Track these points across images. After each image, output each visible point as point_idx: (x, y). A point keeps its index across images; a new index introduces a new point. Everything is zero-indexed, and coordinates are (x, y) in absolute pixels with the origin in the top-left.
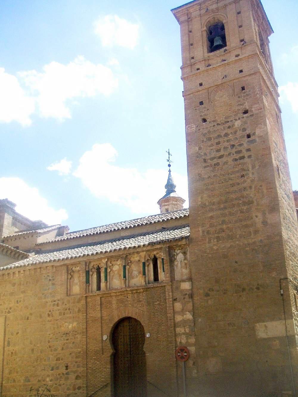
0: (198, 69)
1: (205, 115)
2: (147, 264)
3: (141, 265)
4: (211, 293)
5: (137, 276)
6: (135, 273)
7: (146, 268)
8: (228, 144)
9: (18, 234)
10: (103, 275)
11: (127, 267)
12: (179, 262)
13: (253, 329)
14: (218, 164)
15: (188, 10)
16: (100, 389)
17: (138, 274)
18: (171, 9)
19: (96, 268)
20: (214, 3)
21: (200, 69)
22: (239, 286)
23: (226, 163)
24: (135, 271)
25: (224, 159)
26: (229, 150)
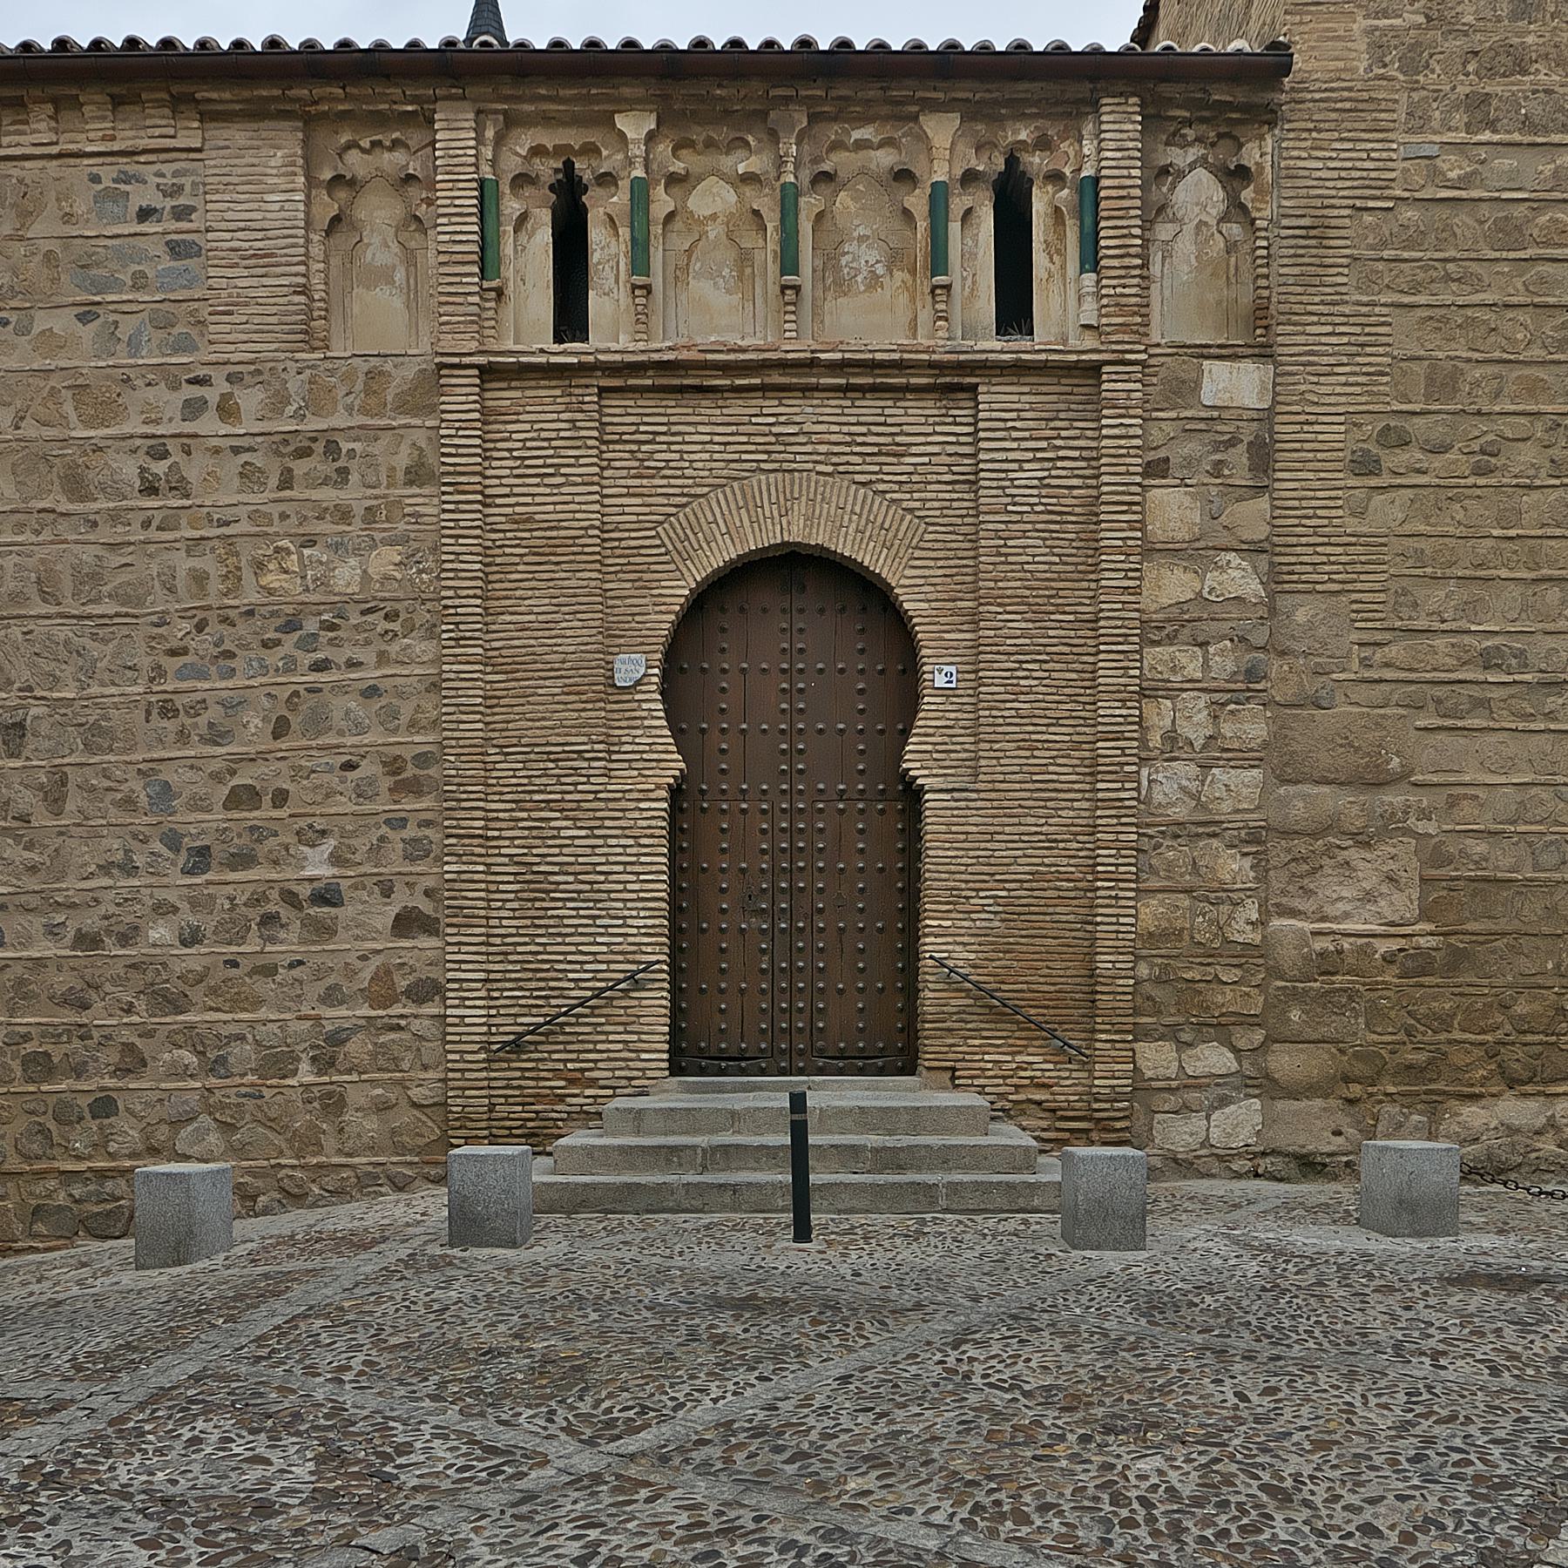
3: (917, 202)
4: (1395, 459)
5: (874, 281)
6: (863, 257)
7: (955, 227)
11: (810, 204)
12: (1189, 229)
17: (880, 270)
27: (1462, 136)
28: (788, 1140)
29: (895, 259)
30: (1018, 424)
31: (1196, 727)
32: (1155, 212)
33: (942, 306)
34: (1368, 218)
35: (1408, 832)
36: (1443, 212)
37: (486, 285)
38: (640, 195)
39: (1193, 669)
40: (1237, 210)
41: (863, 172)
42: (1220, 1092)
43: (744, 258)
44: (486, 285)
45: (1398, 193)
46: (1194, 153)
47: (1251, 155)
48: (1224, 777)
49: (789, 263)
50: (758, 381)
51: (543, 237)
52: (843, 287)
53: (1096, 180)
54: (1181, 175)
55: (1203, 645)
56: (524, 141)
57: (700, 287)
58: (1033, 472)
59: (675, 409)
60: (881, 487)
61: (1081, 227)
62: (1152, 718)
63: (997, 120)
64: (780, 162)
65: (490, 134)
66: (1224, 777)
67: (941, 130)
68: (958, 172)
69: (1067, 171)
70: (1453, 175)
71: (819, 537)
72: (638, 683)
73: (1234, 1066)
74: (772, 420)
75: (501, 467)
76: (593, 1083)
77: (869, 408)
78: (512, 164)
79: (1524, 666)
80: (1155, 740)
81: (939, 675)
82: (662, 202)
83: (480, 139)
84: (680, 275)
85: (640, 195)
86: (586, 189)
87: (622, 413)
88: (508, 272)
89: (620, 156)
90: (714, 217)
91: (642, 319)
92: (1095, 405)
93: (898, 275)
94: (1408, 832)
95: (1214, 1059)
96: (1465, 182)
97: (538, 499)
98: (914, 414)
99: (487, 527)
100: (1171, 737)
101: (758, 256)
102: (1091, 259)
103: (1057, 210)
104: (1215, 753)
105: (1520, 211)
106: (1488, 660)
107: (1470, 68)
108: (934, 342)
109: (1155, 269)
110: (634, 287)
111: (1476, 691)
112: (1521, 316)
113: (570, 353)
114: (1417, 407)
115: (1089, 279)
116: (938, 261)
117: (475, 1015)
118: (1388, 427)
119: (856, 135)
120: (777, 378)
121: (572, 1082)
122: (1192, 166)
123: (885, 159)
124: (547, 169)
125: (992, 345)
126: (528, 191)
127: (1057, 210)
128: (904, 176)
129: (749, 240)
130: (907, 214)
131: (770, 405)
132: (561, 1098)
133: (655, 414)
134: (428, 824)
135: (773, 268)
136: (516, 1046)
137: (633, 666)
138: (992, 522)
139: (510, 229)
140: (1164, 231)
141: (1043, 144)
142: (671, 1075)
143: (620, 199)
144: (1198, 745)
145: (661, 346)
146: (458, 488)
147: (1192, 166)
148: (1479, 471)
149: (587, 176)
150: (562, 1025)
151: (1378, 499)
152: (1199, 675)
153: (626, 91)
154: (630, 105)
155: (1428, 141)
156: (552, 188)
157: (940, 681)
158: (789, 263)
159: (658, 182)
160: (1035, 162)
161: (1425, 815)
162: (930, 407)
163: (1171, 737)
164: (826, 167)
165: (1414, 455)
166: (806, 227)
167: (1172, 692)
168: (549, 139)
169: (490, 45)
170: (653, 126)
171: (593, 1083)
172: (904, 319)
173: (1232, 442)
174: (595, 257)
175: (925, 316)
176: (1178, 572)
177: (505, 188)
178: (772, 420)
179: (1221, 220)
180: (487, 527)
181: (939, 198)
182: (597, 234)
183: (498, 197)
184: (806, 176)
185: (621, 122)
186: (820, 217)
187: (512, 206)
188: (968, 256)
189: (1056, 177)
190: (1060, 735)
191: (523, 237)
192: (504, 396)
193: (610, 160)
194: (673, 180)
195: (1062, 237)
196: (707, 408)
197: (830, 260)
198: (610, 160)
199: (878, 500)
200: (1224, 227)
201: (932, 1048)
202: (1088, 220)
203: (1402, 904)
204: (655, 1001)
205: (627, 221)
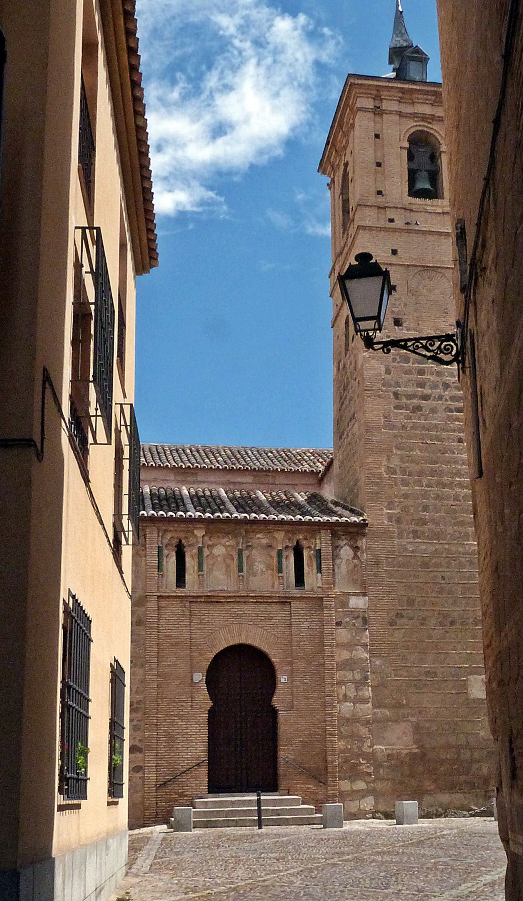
0: (391, 221)
1: (399, 313)
2: (284, 554)
3: (274, 553)
4: (400, 621)
5: (262, 573)
6: (259, 566)
7: (284, 560)
8: (438, 379)
9: (217, 514)
10: (190, 562)
11: (245, 553)
12: (344, 561)
13: (465, 685)
14: (418, 408)
15: (378, 90)
16: (183, 773)
17: (264, 570)
18: (329, 294)
19: (174, 545)
20: (428, 102)
21: (396, 222)
22: (445, 617)
23: (433, 411)
24: (259, 562)
25: (431, 403)
26: (439, 391)
27: (412, 540)
28: (257, 808)
29: (269, 567)
30: (302, 612)
31: (352, 694)
32: (335, 557)
33: (281, 581)
34: (390, 560)
35: (408, 721)
36: (408, 559)
37: (160, 573)
38: (200, 550)
39: (350, 677)
40: (356, 557)
41: (259, 545)
42: (362, 794)
43: (228, 566)
44: (160, 573)
45: (397, 554)
46: (345, 542)
47: (359, 544)
48: (360, 706)
49: (240, 570)
50: (233, 600)
51: (173, 559)
52: (255, 575)
53: (320, 550)
54: (342, 547)
55: (353, 670)
56: (169, 536)
57: (216, 573)
58: (306, 625)
59: (210, 607)
60: (266, 628)
61: (317, 561)
62: (340, 691)
63: (294, 534)
64: (238, 543)
65: (161, 534)
66: (360, 706)
67: (280, 536)
68: (285, 546)
69: (313, 546)
70: (411, 549)
71: (249, 642)
72: (200, 681)
73: (366, 787)
74: (236, 610)
75: (162, 622)
76: (186, 796)
77: (262, 607)
78: (166, 541)
79: (436, 675)
80: (341, 697)
81: (283, 679)
82: (206, 552)
83: (158, 536)
84: (210, 571)
85: (200, 550)
86: (185, 547)
87: (196, 607)
88: (165, 570)
89: (195, 540)
90: (220, 555)
91: (201, 584)
92: (321, 607)
93: (269, 571)
94: (408, 721)
95: (361, 785)
96: (413, 551)
97: (173, 631)
98: (274, 608)
99: (159, 638)
100: (345, 695)
101: (232, 566)
102: (319, 569)
103: (310, 556)
104: (357, 700)
105: (427, 559)
106: (427, 673)
107: (413, 523)
108: (278, 590)
109: (336, 571)
110: (199, 575)
111: (424, 682)
112: (430, 585)
113: (180, 592)
114: (405, 608)
115: (319, 575)
116: (280, 570)
117: (153, 776)
118: (397, 613)
119: (258, 536)
120: (238, 600)
121: (180, 796)
122: (345, 545)
123: (265, 541)
124: (175, 542)
125: (295, 592)
126: (169, 547)
127: (310, 556)
128: (270, 546)
129: (229, 561)
130: (271, 557)
131: (236, 606)
132: (177, 801)
133: (204, 608)
134: (139, 721)
135: (236, 570)
136: (165, 784)
137: (199, 677)
138: (295, 638)
139: (165, 558)
140: (338, 561)
141: (306, 539)
142: (209, 793)
143: (195, 551)
144: (352, 697)
145: (206, 591)
146: (151, 628)
147: (345, 545)
148: (422, 624)
149: (185, 544)
150: (178, 779)
151: (396, 632)
152: (352, 679)
153: (198, 526)
154: (197, 528)
155: (404, 541)
156: (175, 547)
157: (283, 680)
158: (240, 570)
159: (205, 547)
160: (304, 543)
161: (413, 716)
162: (278, 607)
163: (345, 695)
164: (250, 544)
165: (404, 620)
166: (245, 560)
167: (344, 683)
168: (176, 535)
169: (163, 515)
170: (204, 533)
171: (186, 796)
172: (271, 583)
173: (358, 617)
174: (187, 565)
175: (276, 583)
176: (345, 651)
177: (164, 547)
178: (236, 610)
179: (353, 559)
180: (159, 638)
181: (280, 553)
182: (188, 559)
183: (162, 550)
184: (244, 546)
185: (195, 532)
186: (248, 557)
187: (166, 552)
188: (287, 567)
189: (309, 547)
190: (315, 695)
191: (168, 560)
192: (164, 603)
193: (192, 541)
194: (209, 546)
195: (311, 562)
196: (219, 606)
197: (251, 567)
198: (192, 541)
199: (265, 631)
200: (353, 561)
201: (283, 784)
202: (319, 561)
203: (408, 739)
204: (204, 771)
205: (197, 556)
